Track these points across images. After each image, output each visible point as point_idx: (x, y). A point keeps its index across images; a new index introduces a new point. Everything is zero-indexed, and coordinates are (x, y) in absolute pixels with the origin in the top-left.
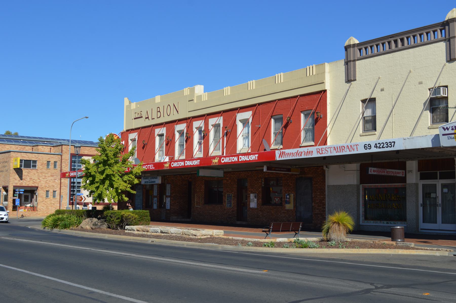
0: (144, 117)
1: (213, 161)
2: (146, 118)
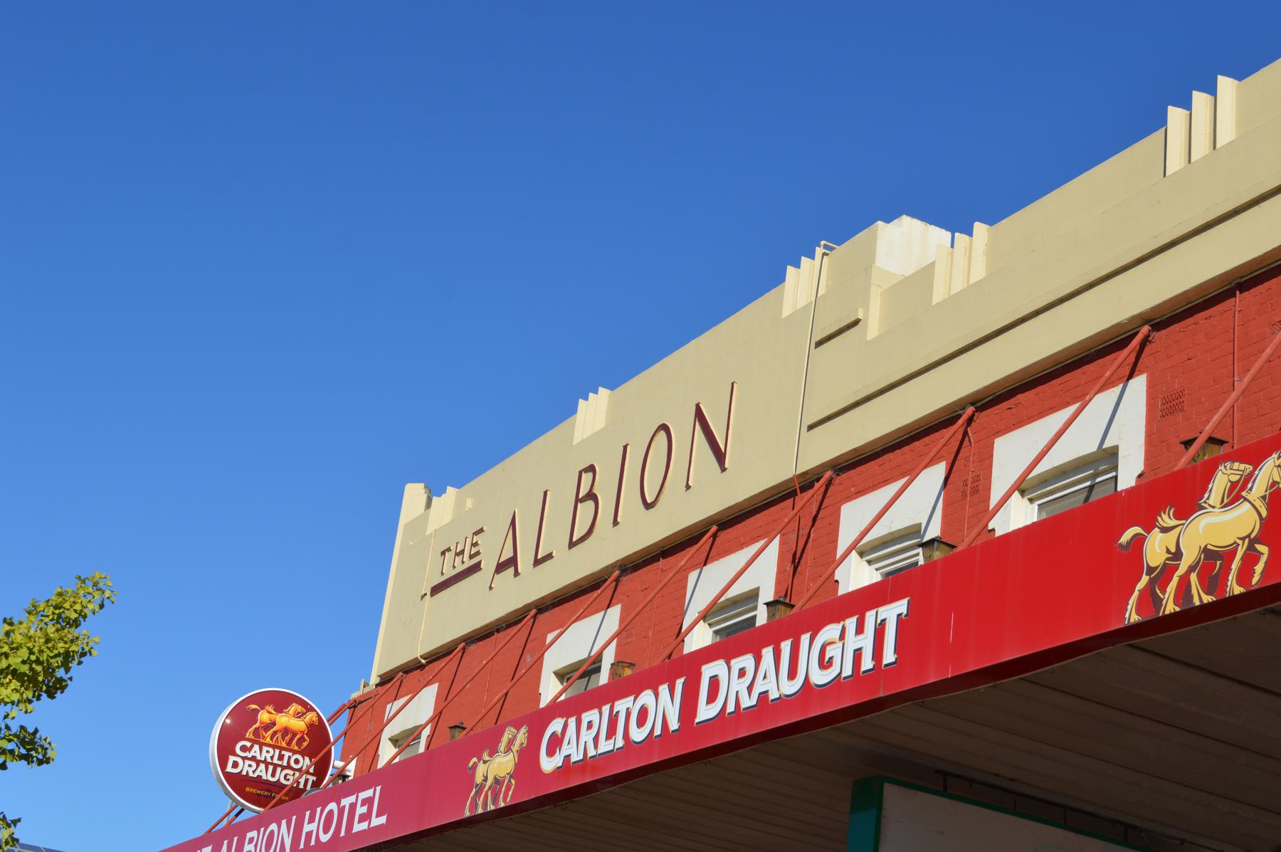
0: (489, 565)
1: (1156, 549)
2: (501, 568)
